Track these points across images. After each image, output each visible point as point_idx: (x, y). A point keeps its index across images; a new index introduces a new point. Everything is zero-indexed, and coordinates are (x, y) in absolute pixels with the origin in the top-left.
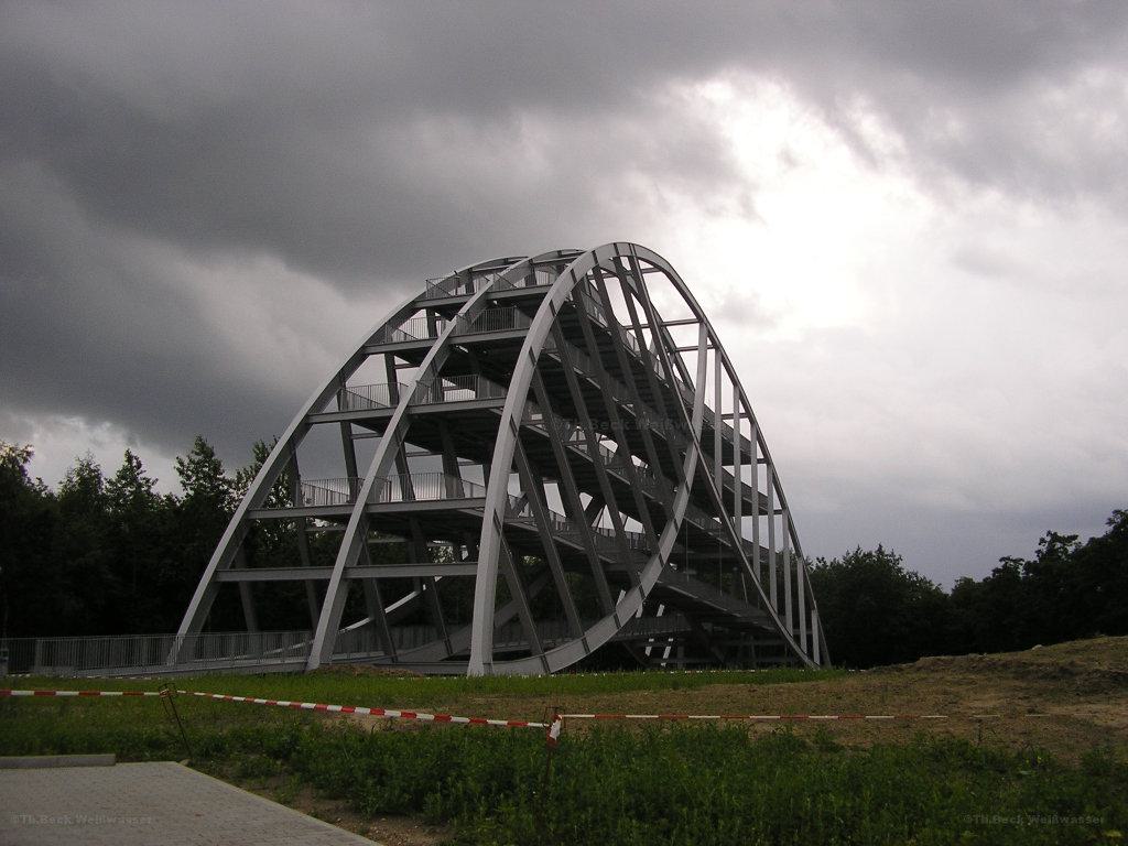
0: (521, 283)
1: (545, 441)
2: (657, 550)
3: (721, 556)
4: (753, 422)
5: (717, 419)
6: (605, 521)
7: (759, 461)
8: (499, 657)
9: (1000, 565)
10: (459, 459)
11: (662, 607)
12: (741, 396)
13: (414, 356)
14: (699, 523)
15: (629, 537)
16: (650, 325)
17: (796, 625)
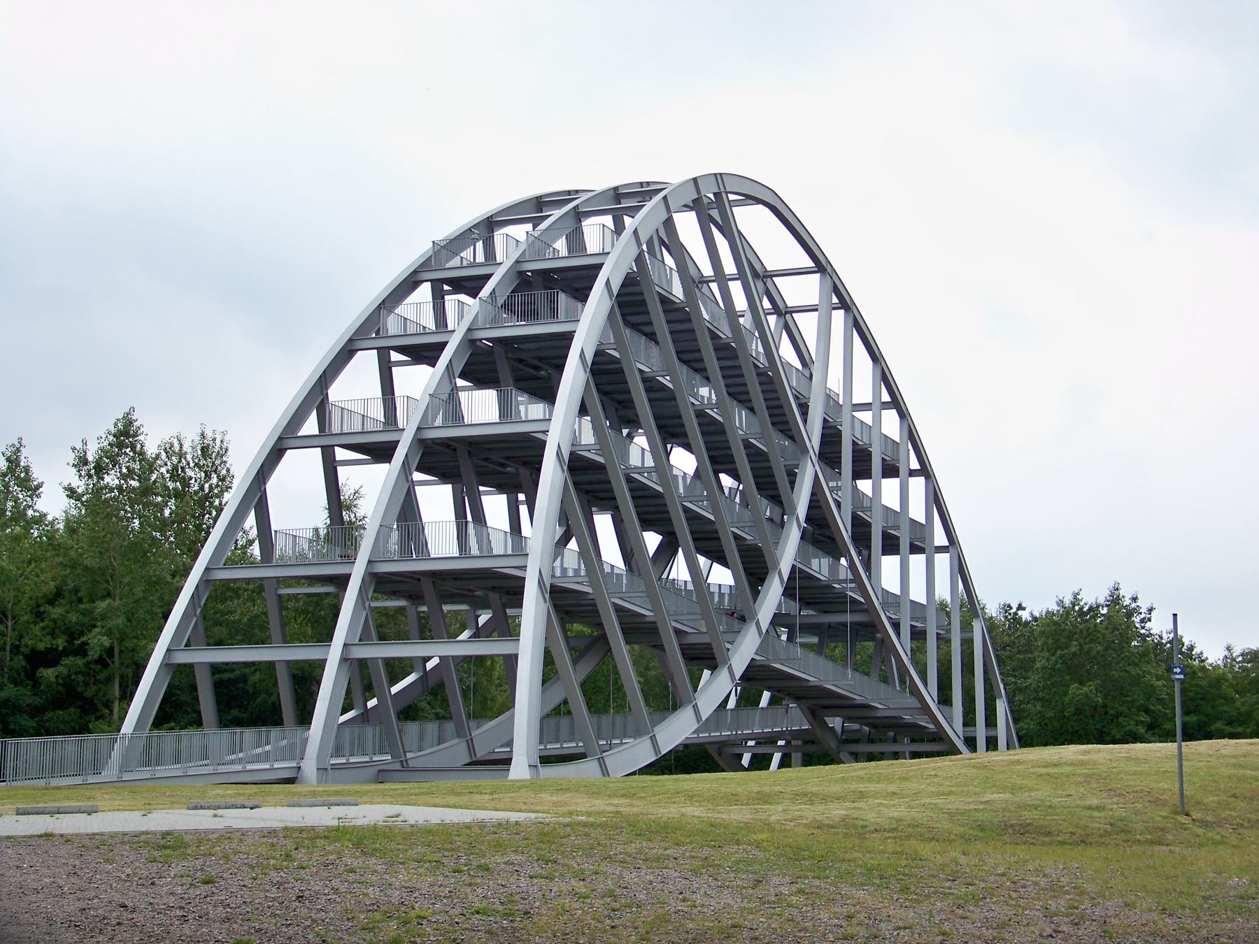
0: (561, 245)
1: (600, 468)
2: (754, 615)
3: (849, 618)
4: (903, 414)
5: (846, 411)
6: (679, 570)
7: (912, 473)
8: (546, 760)
9: (1054, 607)
10: (482, 488)
11: (766, 696)
12: (885, 378)
13: (424, 353)
14: (820, 567)
15: (607, 569)
16: (741, 276)
17: (969, 720)
